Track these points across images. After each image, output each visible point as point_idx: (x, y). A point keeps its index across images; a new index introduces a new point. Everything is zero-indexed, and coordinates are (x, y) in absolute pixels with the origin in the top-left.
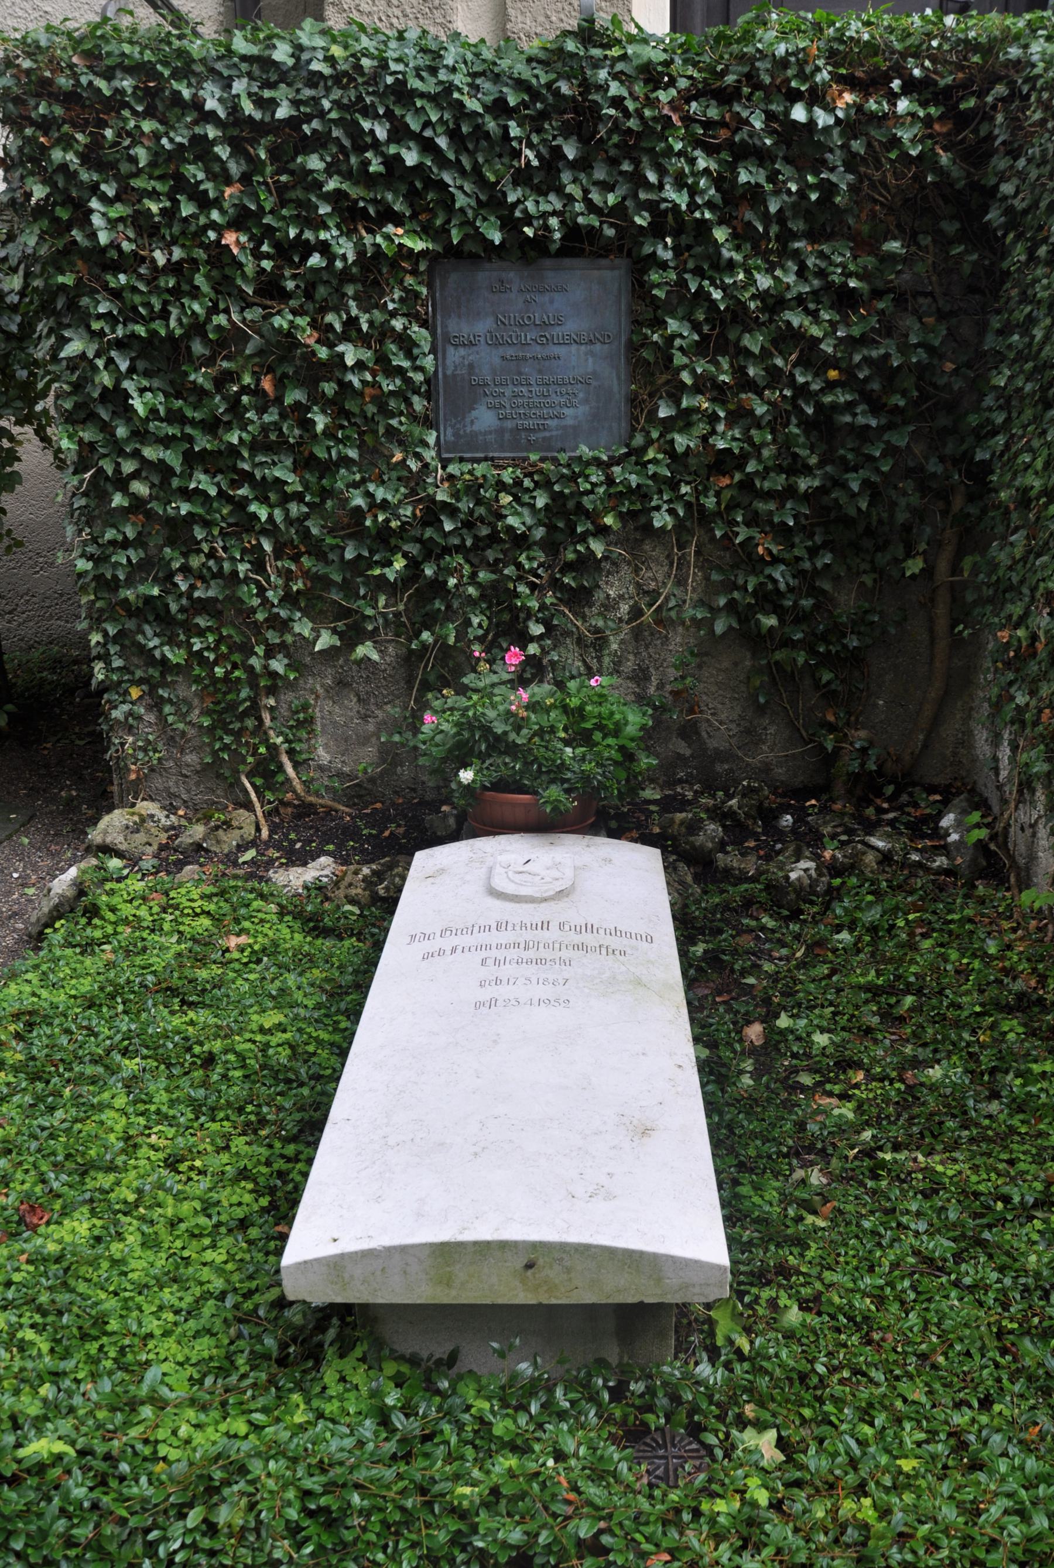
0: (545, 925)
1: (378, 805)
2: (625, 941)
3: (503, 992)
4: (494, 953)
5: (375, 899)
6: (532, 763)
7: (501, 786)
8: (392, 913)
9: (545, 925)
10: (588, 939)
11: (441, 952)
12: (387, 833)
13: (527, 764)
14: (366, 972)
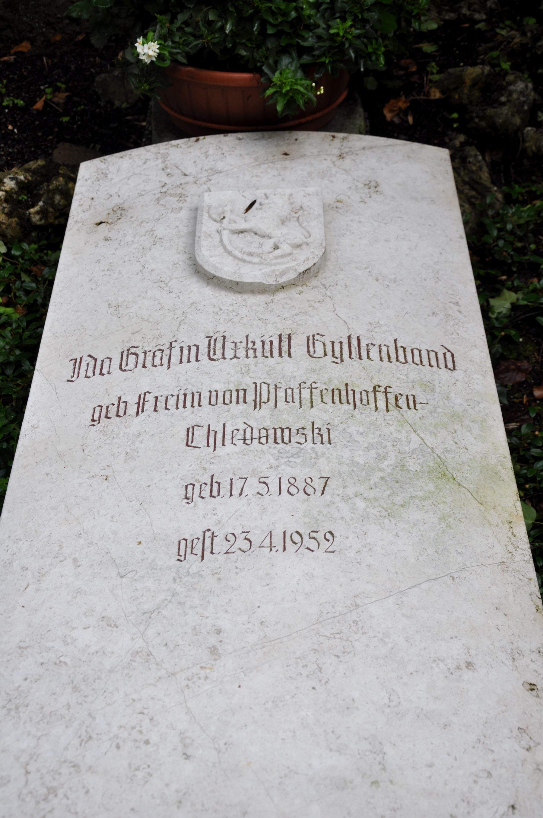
0: (283, 345)
1: (25, 47)
2: (413, 372)
3: (224, 514)
4: (207, 415)
5: (26, 229)
6: (251, 19)
7: (203, 59)
8: (57, 247)
9: (283, 345)
10: (356, 374)
11: (120, 408)
12: (39, 105)
13: (243, 22)
14: (18, 364)
